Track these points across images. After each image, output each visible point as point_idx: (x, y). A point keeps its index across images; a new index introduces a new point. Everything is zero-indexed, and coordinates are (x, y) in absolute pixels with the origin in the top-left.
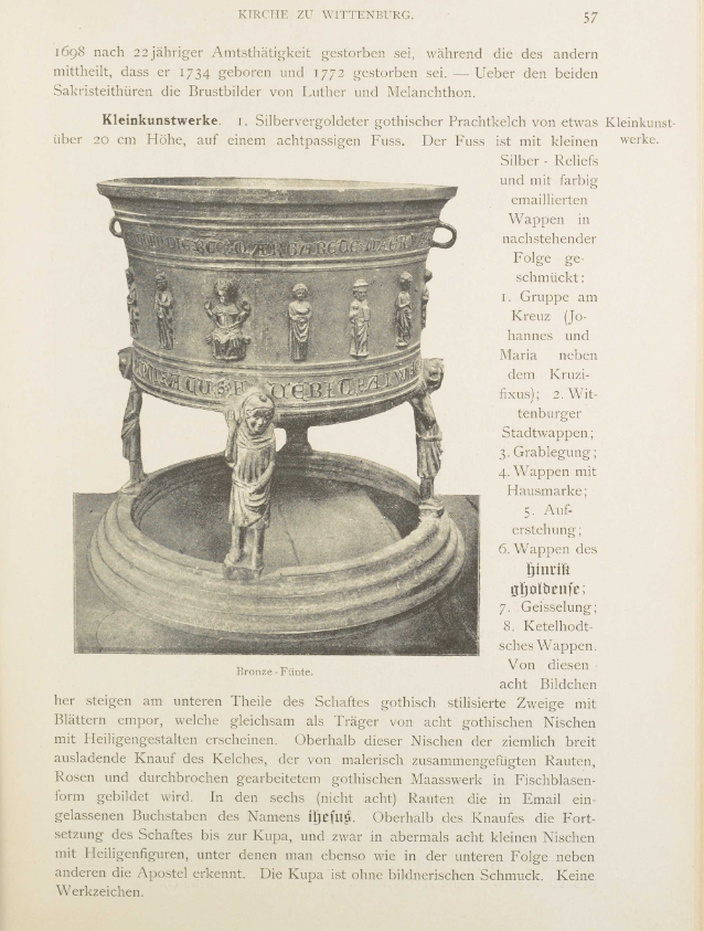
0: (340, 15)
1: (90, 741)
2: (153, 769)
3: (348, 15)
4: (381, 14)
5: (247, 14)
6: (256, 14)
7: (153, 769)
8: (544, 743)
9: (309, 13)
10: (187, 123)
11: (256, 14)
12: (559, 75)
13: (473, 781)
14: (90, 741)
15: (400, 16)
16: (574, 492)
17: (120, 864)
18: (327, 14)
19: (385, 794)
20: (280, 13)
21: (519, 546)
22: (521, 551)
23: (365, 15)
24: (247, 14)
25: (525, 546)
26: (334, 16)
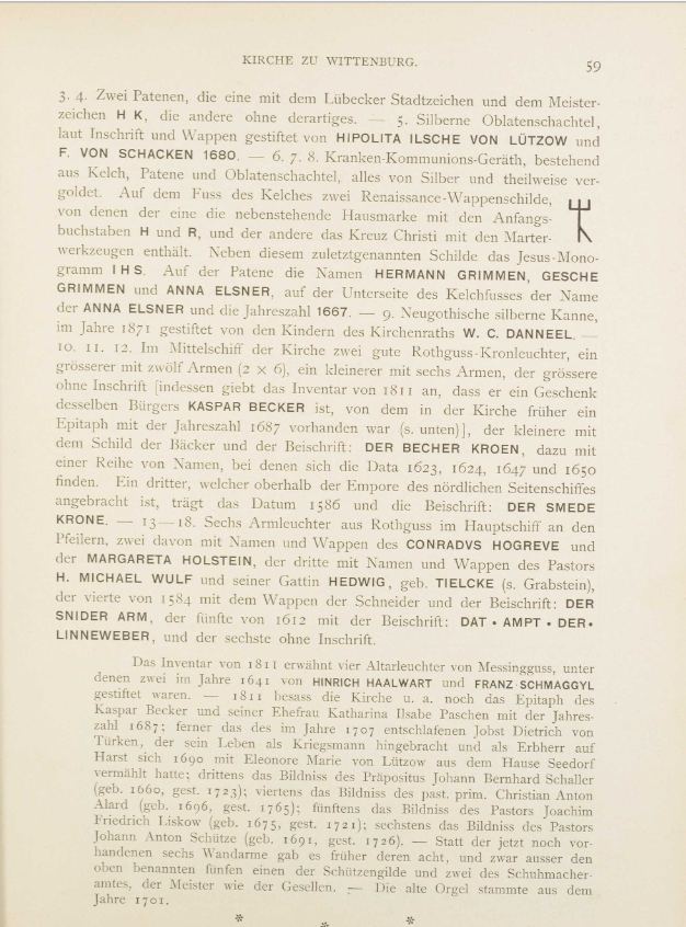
0: (344, 62)
1: (470, 528)
2: (191, 456)
3: (352, 62)
4: (384, 62)
5: (251, 60)
6: (261, 60)
7: (191, 456)
8: (80, 115)
9: (314, 59)
10: (115, 98)
11: (261, 60)
12: (539, 162)
13: (80, 251)
14: (470, 528)
15: (404, 62)
16: (201, 447)
17: (154, 417)
18: (331, 60)
19: (576, 118)
20: (285, 59)
21: (459, 561)
22: (462, 567)
23: (369, 61)
24: (251, 60)
25: (465, 561)
26: (338, 61)
